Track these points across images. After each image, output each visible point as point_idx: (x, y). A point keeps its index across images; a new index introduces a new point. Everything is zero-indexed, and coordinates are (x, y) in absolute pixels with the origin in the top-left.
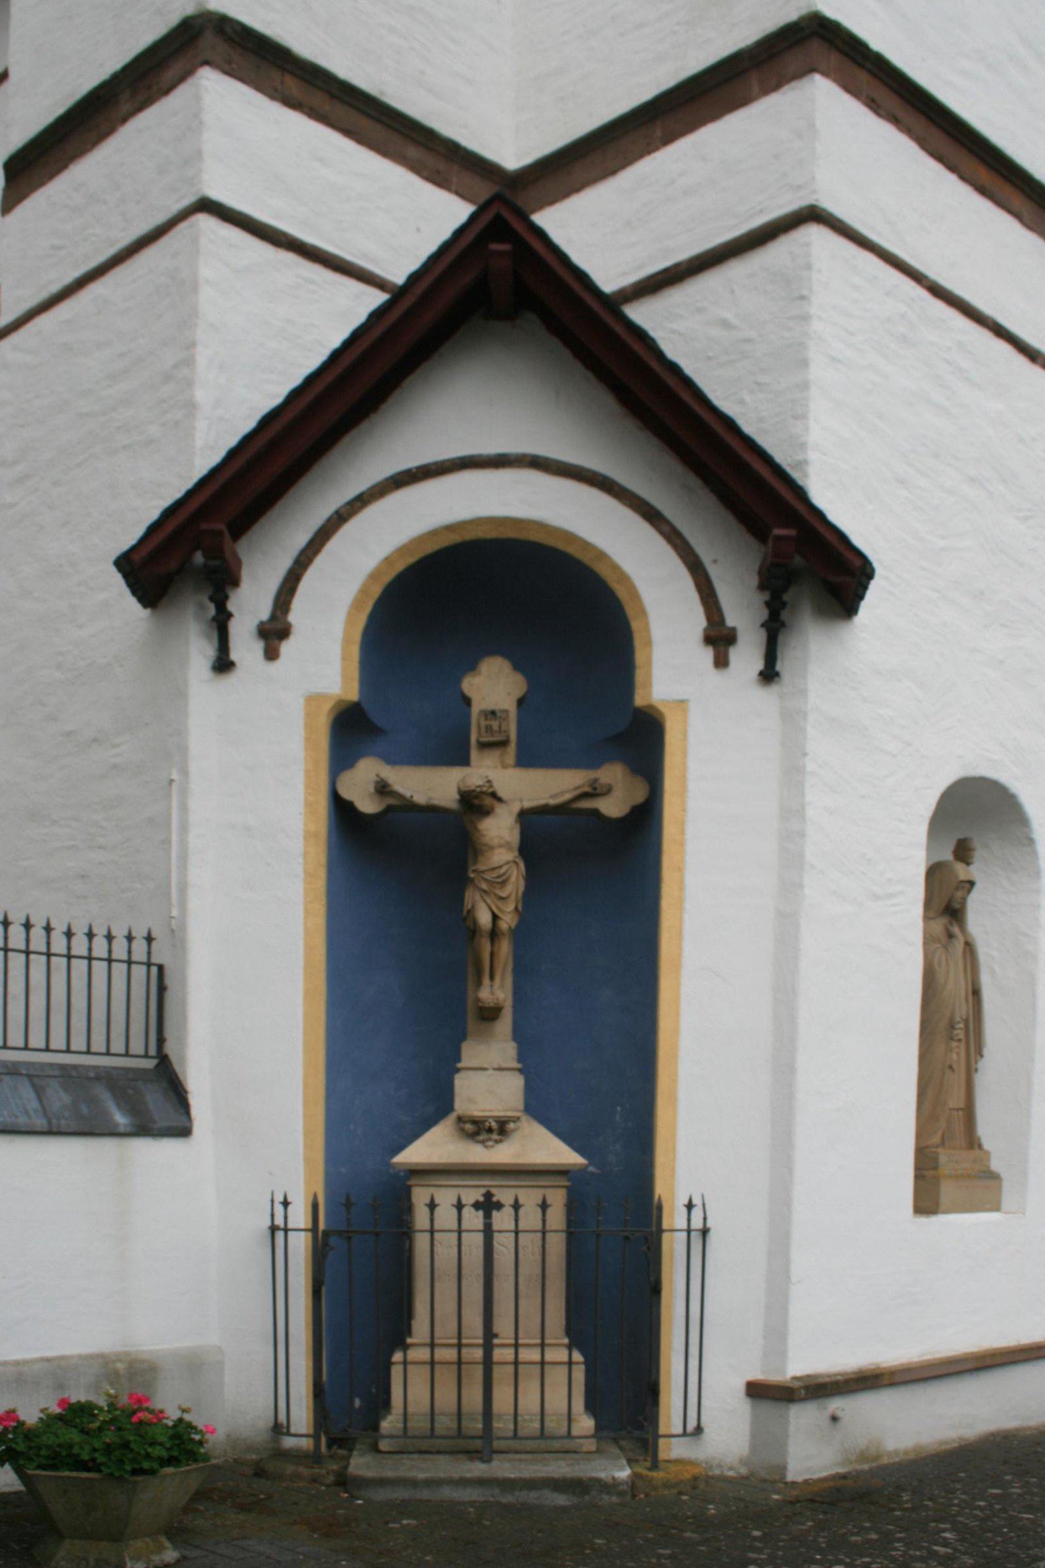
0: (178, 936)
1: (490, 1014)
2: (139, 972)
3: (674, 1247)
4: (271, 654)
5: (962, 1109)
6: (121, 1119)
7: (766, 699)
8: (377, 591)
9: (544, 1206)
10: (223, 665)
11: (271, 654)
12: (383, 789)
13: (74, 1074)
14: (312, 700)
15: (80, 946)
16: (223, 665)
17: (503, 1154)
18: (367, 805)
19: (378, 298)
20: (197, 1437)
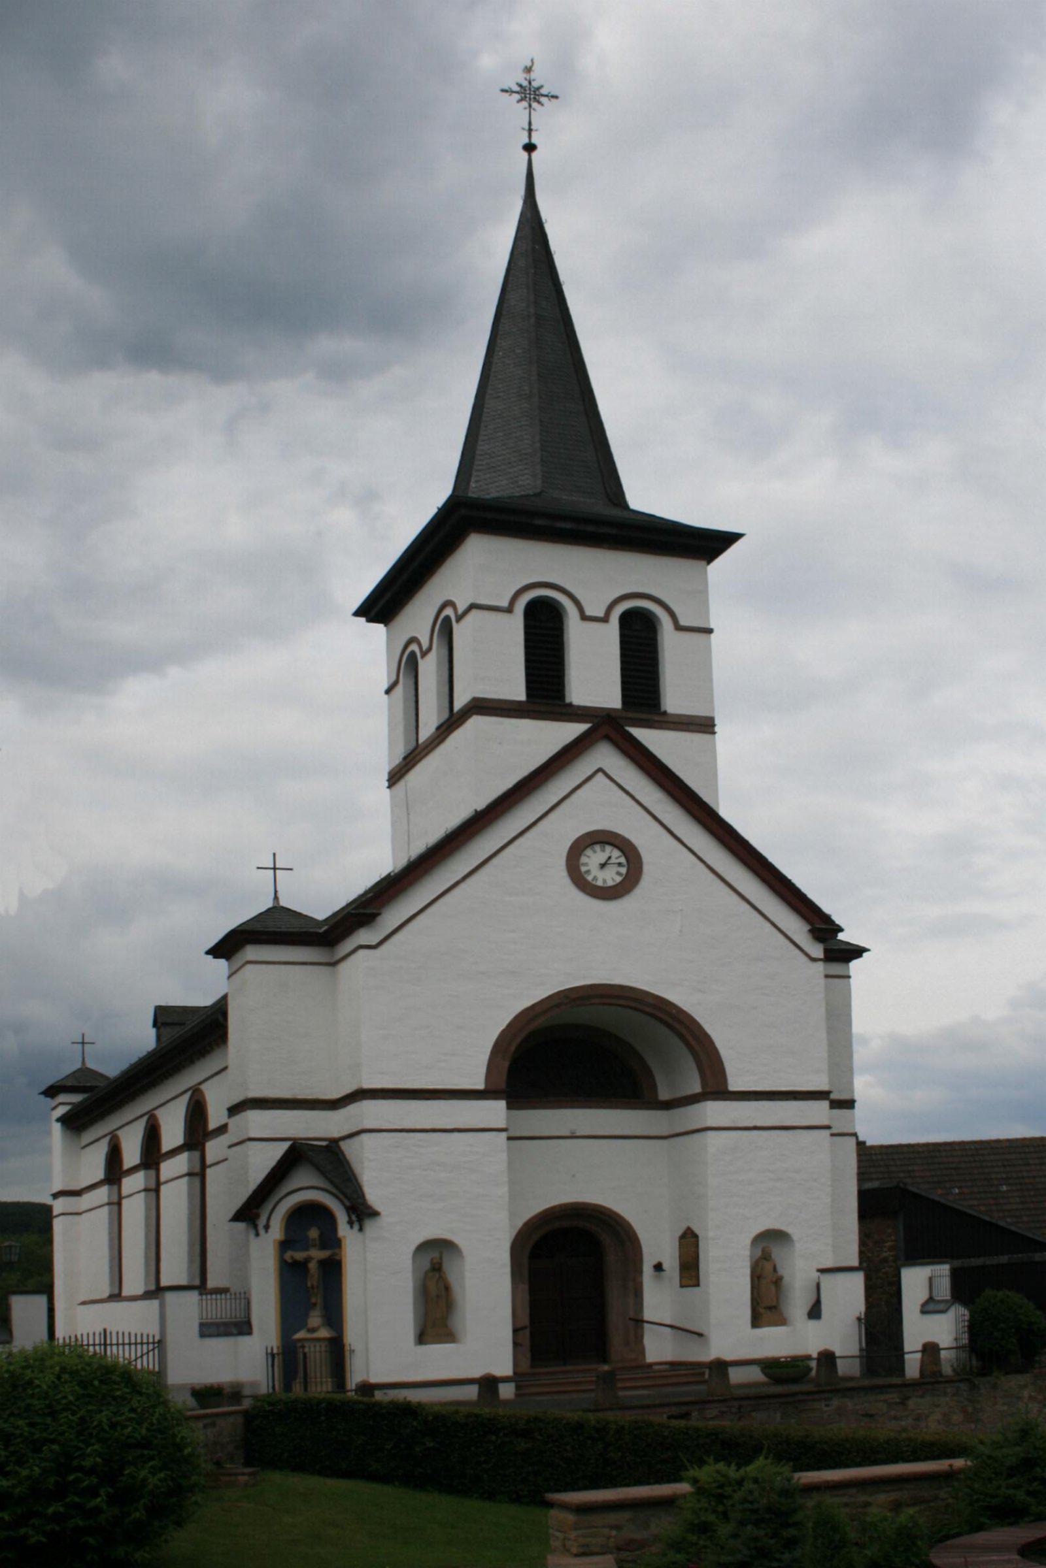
0: (250, 1294)
1: (315, 1304)
2: (243, 1301)
3: (347, 1354)
4: (267, 1231)
5: (353, 1390)
6: (235, 1332)
7: (359, 1235)
8: (286, 1216)
9: (320, 1346)
10: (257, 1234)
11: (267, 1231)
12: (292, 1257)
13: (957, 1148)
14: (275, 1241)
15: (238, 1296)
16: (257, 1234)
17: (316, 1335)
18: (290, 1261)
19: (527, 1332)
20: (189, 1440)
